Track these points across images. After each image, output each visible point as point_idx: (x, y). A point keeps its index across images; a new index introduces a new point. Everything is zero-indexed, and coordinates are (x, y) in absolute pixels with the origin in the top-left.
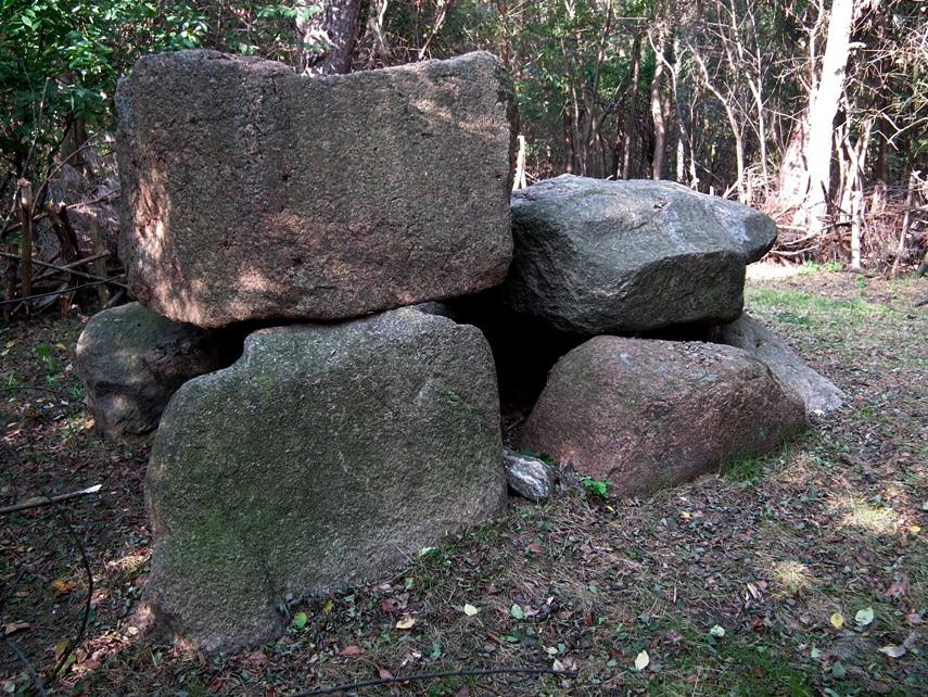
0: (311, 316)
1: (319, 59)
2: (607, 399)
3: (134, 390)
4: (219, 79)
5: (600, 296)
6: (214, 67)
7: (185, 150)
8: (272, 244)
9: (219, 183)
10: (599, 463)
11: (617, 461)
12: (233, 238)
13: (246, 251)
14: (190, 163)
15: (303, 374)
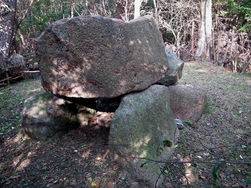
0: (138, 90)
1: (6, 14)
2: (185, 101)
3: (49, 123)
4: (108, 24)
5: (172, 76)
6: (106, 20)
7: (101, 46)
8: (130, 71)
9: (113, 55)
10: (186, 116)
11: (191, 115)
12: (120, 70)
13: (124, 74)
14: (103, 49)
15: (147, 106)
